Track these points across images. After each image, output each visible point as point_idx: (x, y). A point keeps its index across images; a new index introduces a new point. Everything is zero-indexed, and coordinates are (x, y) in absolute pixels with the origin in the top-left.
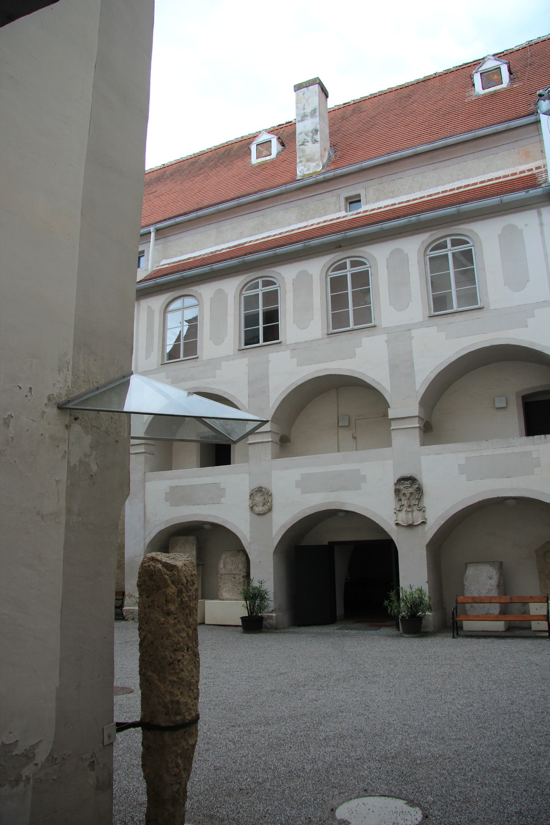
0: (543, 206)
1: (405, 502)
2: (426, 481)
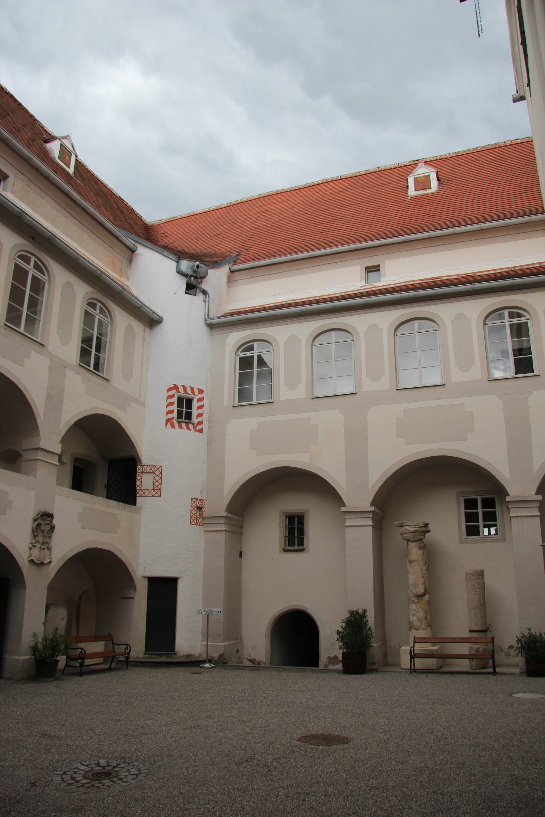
1: (40, 538)
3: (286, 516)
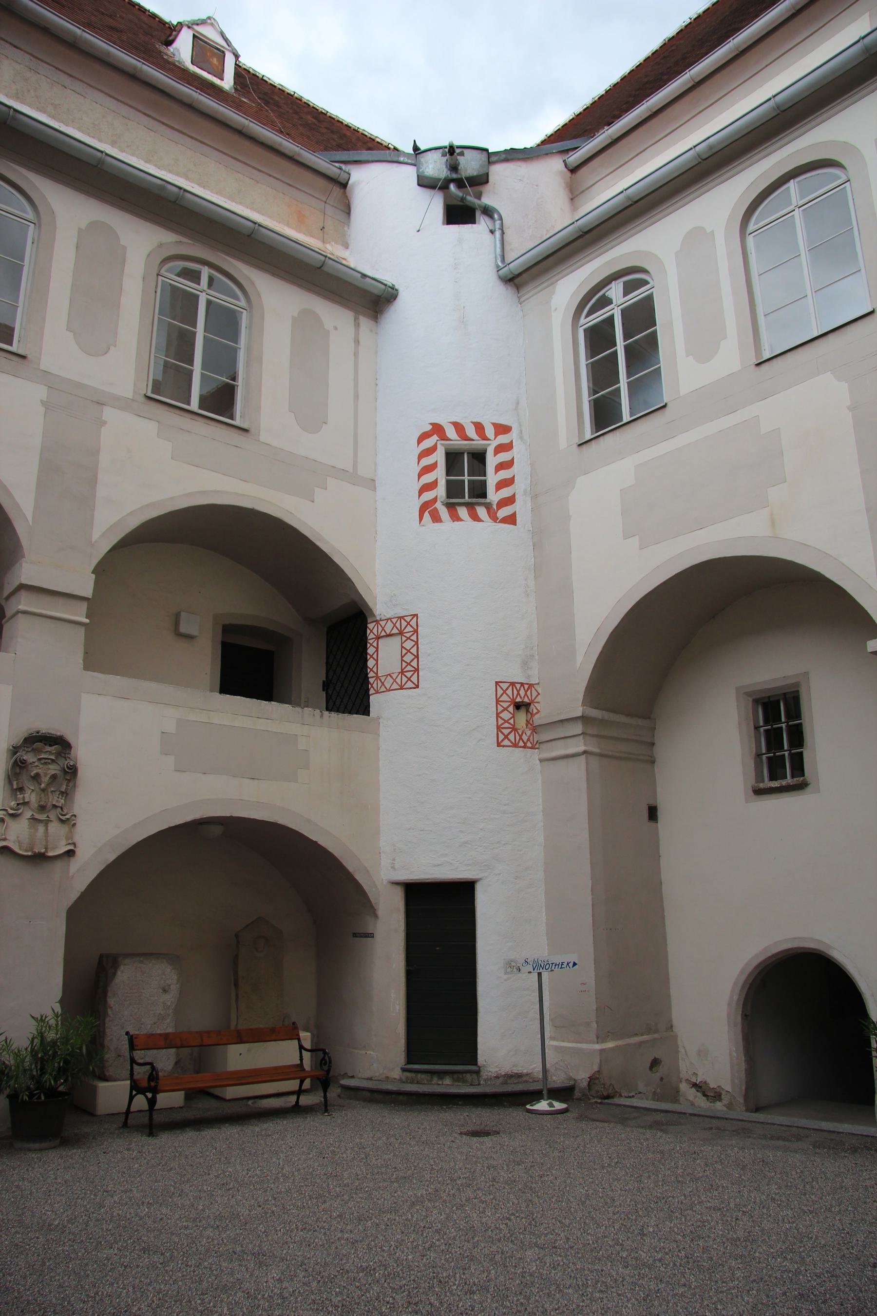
0: (365, 315)
1: (31, 796)
2: (86, 753)
3: (756, 701)
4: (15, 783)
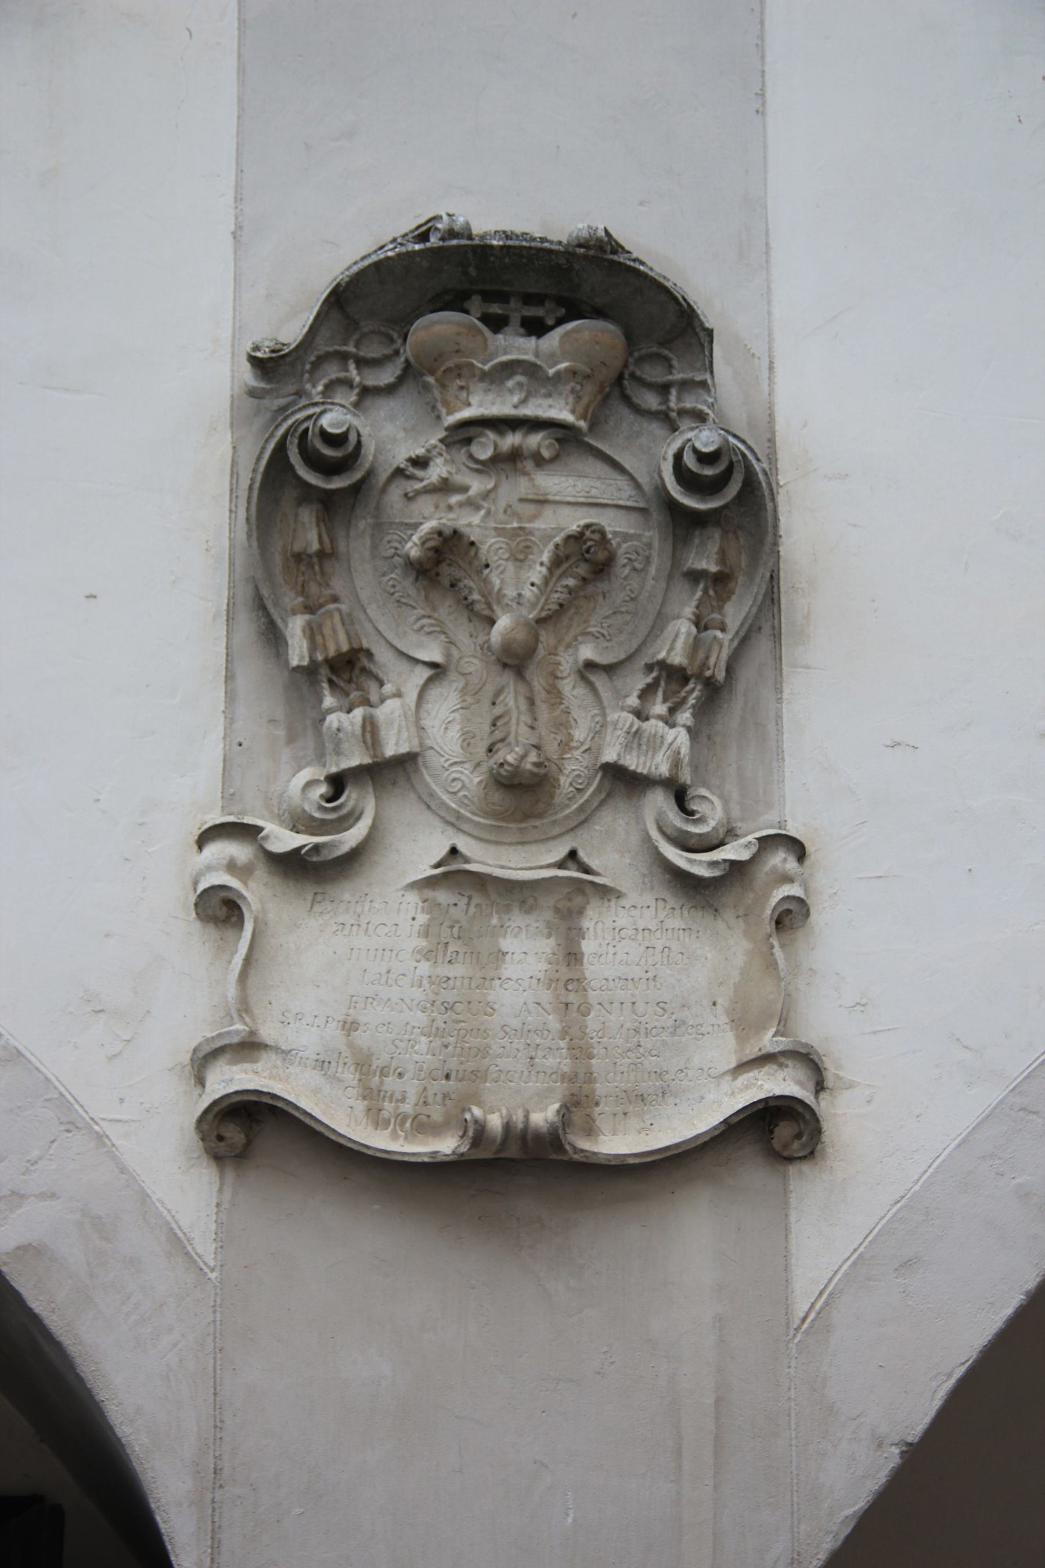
1: (431, 714)
2: (813, 375)
4: (295, 628)
